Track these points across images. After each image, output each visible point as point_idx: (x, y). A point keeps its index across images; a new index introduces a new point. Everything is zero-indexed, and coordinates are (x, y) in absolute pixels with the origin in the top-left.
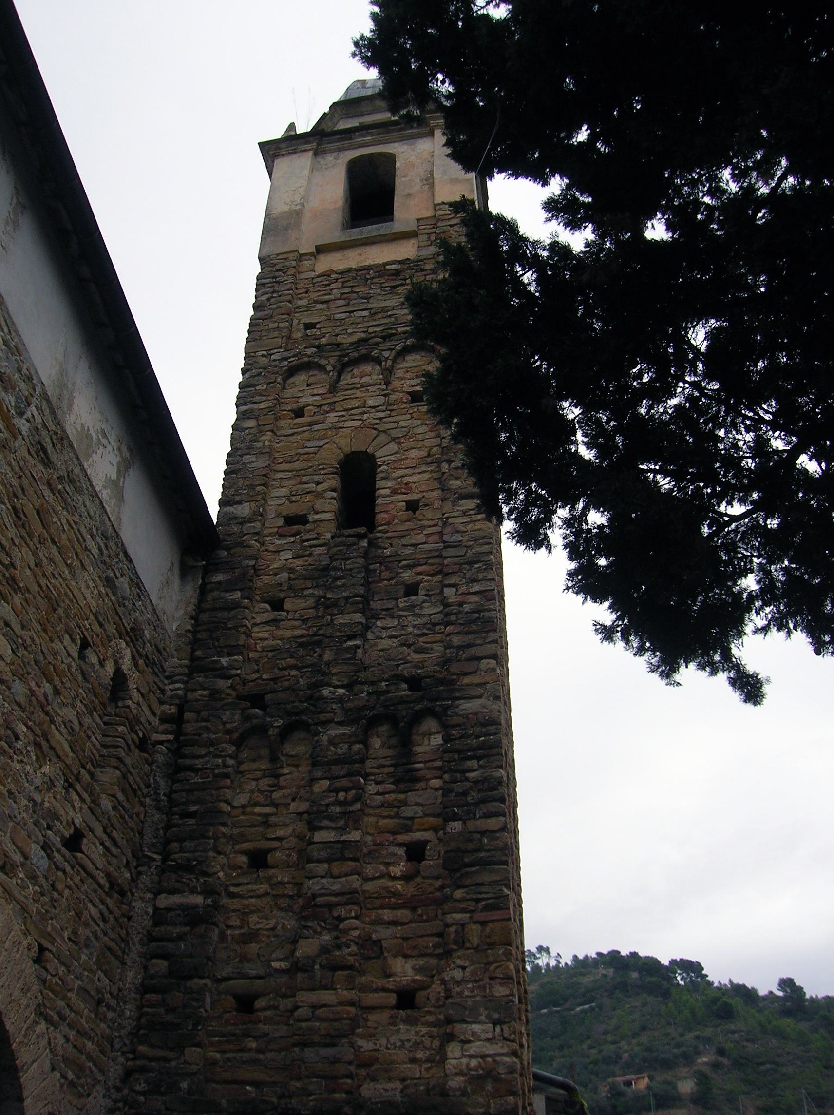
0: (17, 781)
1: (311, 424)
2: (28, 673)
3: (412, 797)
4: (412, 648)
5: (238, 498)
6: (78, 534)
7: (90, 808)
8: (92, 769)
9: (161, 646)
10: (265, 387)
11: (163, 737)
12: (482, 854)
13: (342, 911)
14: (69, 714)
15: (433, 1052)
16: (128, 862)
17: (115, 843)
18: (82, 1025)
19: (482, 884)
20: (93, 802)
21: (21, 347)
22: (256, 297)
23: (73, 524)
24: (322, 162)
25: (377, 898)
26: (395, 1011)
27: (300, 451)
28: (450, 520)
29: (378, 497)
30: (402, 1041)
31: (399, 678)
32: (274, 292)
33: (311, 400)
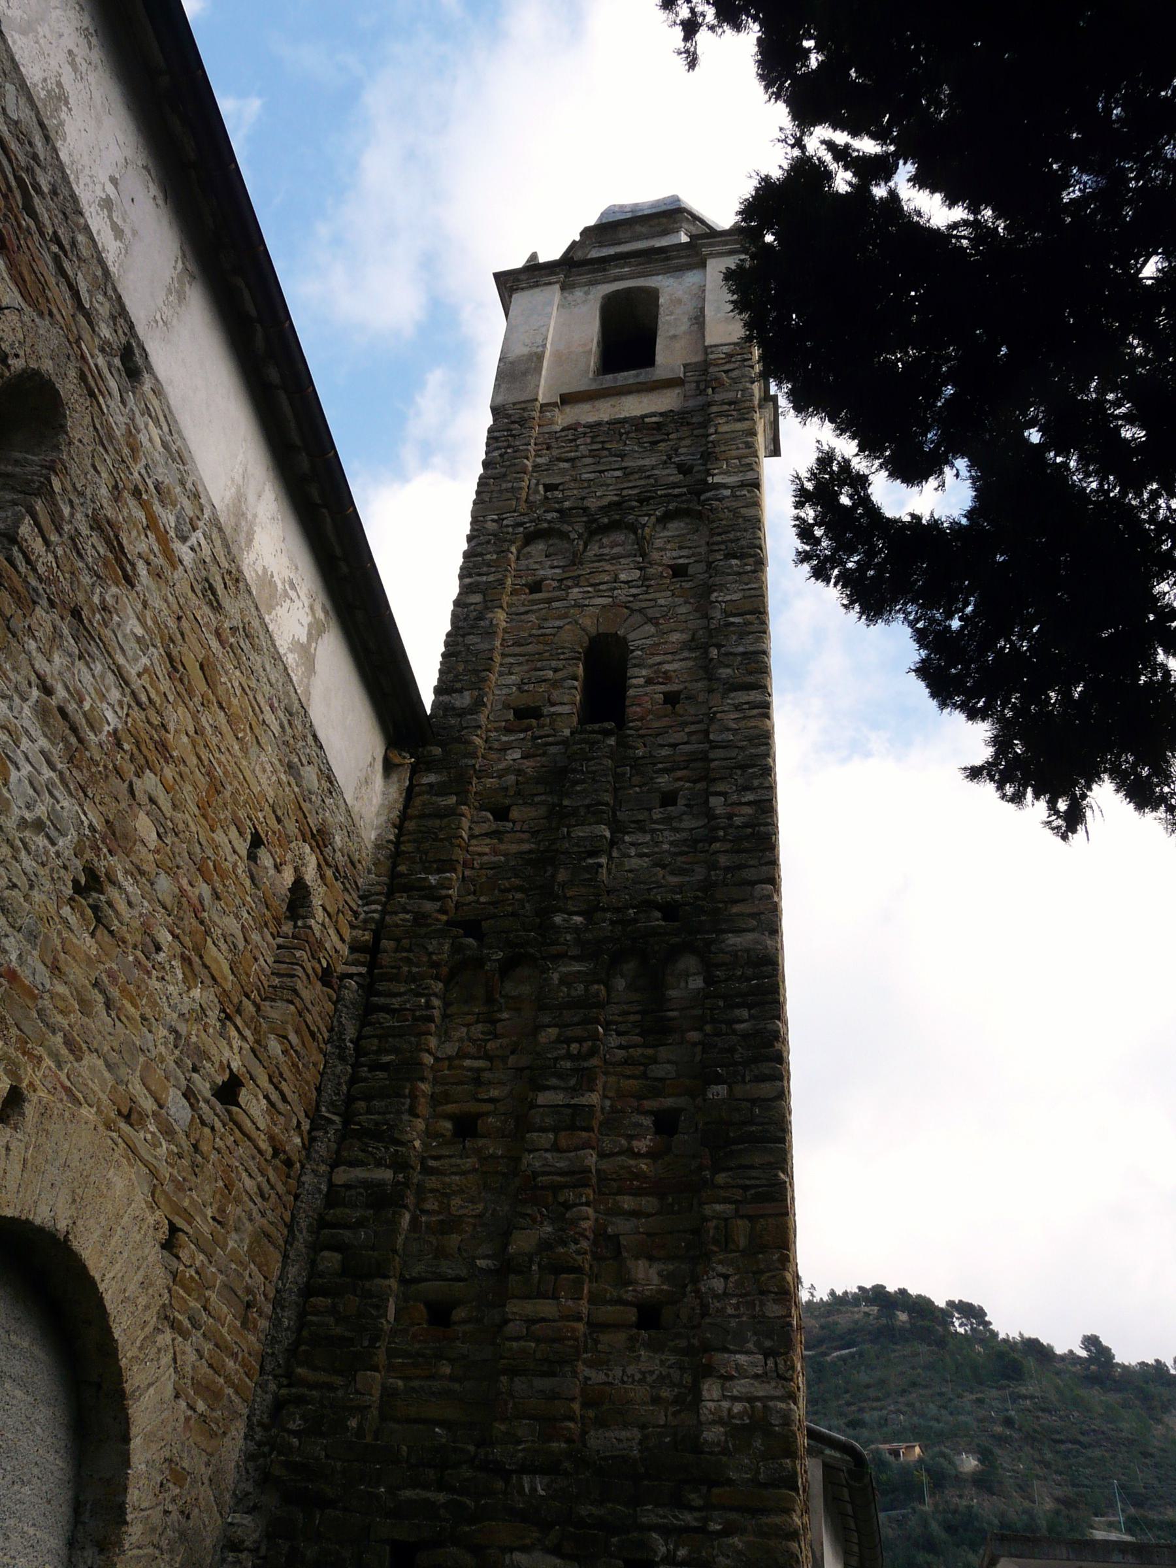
1: (549, 601)
2: (178, 867)
3: (663, 1053)
4: (668, 869)
5: (458, 685)
6: (254, 702)
7: (253, 1050)
8: (258, 999)
9: (356, 857)
10: (495, 557)
11: (354, 970)
12: (754, 1128)
13: (570, 1195)
14: (232, 925)
15: (683, 1390)
16: (299, 1123)
17: (284, 1099)
18: (222, 1335)
19: (752, 1167)
20: (258, 1042)
21: (185, 455)
22: (487, 453)
23: (247, 689)
24: (570, 298)
25: (615, 1180)
26: (635, 1331)
27: (534, 632)
28: (718, 715)
29: (630, 687)
30: (643, 1373)
31: (650, 905)
32: (509, 447)
33: (549, 572)
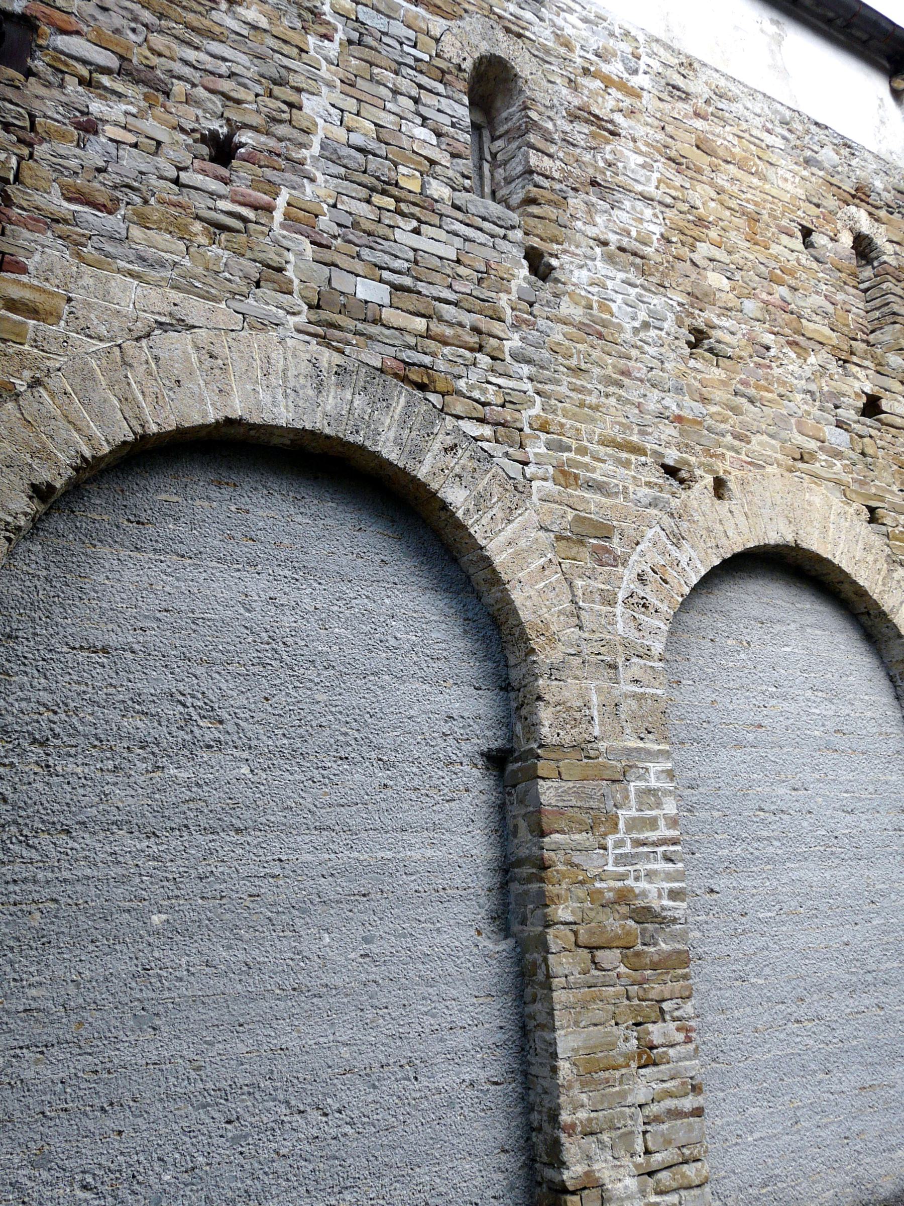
0: (785, 383)
6: (753, 139)
21: (602, 13)
